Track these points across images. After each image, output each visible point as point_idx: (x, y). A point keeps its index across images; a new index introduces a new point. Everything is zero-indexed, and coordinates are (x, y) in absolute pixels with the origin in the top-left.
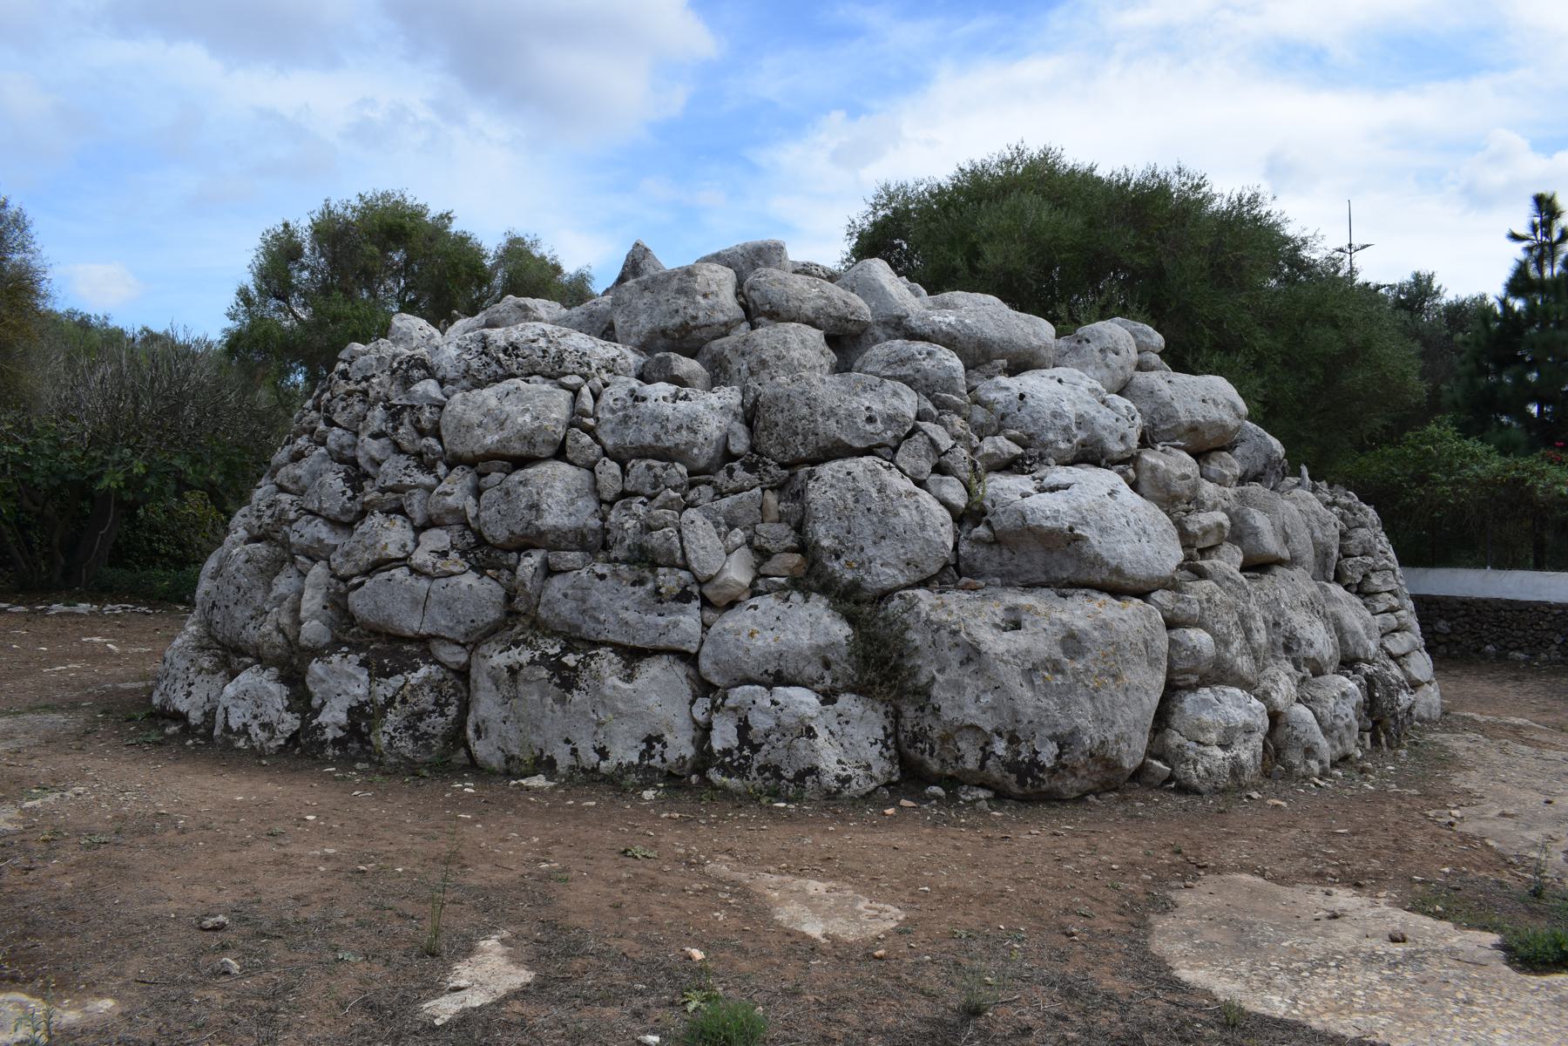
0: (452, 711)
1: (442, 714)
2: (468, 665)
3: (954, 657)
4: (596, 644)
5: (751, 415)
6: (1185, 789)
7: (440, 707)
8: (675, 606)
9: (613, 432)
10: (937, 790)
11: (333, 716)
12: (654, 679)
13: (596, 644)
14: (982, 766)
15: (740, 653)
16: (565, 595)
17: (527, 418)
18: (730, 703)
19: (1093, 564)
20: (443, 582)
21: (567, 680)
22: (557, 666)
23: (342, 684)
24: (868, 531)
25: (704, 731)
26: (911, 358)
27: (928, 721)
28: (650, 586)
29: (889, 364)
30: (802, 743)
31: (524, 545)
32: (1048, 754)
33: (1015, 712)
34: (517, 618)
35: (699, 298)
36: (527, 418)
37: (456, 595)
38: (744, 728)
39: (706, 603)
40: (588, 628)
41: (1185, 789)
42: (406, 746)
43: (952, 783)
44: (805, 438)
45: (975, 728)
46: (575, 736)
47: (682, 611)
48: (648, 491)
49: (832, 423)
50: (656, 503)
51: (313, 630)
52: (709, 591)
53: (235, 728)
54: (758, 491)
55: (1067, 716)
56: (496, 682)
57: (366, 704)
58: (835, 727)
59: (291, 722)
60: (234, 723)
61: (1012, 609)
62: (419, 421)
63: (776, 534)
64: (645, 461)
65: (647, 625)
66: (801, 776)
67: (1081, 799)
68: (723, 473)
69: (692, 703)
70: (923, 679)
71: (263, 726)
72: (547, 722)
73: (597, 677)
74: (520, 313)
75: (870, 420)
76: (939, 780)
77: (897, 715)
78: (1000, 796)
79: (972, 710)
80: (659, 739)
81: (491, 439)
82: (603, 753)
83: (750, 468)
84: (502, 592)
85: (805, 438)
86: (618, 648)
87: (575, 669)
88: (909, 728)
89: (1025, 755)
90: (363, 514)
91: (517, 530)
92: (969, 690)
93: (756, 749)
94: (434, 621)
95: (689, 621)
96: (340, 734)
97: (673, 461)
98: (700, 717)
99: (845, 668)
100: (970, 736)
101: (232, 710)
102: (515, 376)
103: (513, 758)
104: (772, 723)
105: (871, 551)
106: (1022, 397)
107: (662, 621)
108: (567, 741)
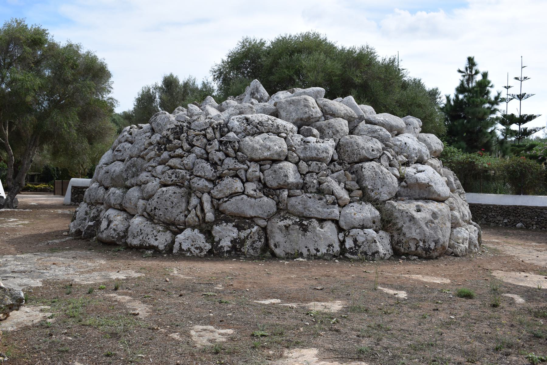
0: (263, 240)
1: (260, 241)
2: (266, 227)
3: (407, 219)
4: (311, 218)
5: (337, 148)
6: (456, 255)
7: (259, 239)
8: (331, 206)
9: (302, 152)
10: (403, 257)
11: (226, 243)
12: (329, 228)
13: (311, 218)
14: (416, 249)
15: (353, 220)
16: (299, 203)
17: (277, 147)
18: (351, 234)
19: (433, 193)
20: (259, 199)
21: (305, 229)
22: (301, 225)
23: (226, 234)
24: (380, 184)
25: (342, 243)
26: (376, 131)
27: (402, 237)
28: (325, 200)
29: (369, 132)
30: (373, 244)
31: (281, 188)
32: (432, 246)
33: (425, 234)
34: (282, 210)
35: (312, 109)
36: (277, 147)
37: (263, 203)
38: (355, 241)
39: (339, 206)
40: (306, 213)
41: (456, 255)
42: (251, 251)
43: (407, 255)
44: (357, 155)
45: (415, 239)
46: (308, 245)
47: (334, 208)
48: (317, 171)
49: (364, 151)
50: (319, 175)
51: (210, 216)
52: (340, 202)
53: (185, 249)
54: (342, 171)
55: (437, 235)
56: (281, 230)
57: (237, 239)
58: (380, 240)
59: (208, 246)
60: (184, 247)
61: (417, 206)
62: (234, 146)
63: (353, 184)
64: (308, 160)
65: (324, 212)
66: (373, 254)
67: (436, 258)
68: (332, 166)
69: (338, 234)
70: (400, 226)
71: (197, 248)
72: (300, 242)
73: (314, 228)
74: (250, 109)
75: (373, 150)
76: (403, 254)
77: (392, 237)
78: (420, 257)
79: (414, 234)
80: (332, 245)
81: (267, 154)
82: (318, 250)
83: (340, 164)
84: (275, 203)
85: (357, 155)
86: (318, 219)
87: (307, 225)
88: (396, 240)
89: (427, 246)
90: (220, 178)
91: (282, 183)
92: (413, 228)
93: (360, 247)
94: (256, 212)
95: (336, 210)
96: (229, 249)
97: (322, 162)
98: (342, 239)
99: (378, 224)
100: (412, 241)
101: (183, 243)
102: (263, 133)
103: (288, 253)
104: (364, 239)
105: (381, 190)
106: (405, 143)
107: (329, 211)
108: (306, 247)
